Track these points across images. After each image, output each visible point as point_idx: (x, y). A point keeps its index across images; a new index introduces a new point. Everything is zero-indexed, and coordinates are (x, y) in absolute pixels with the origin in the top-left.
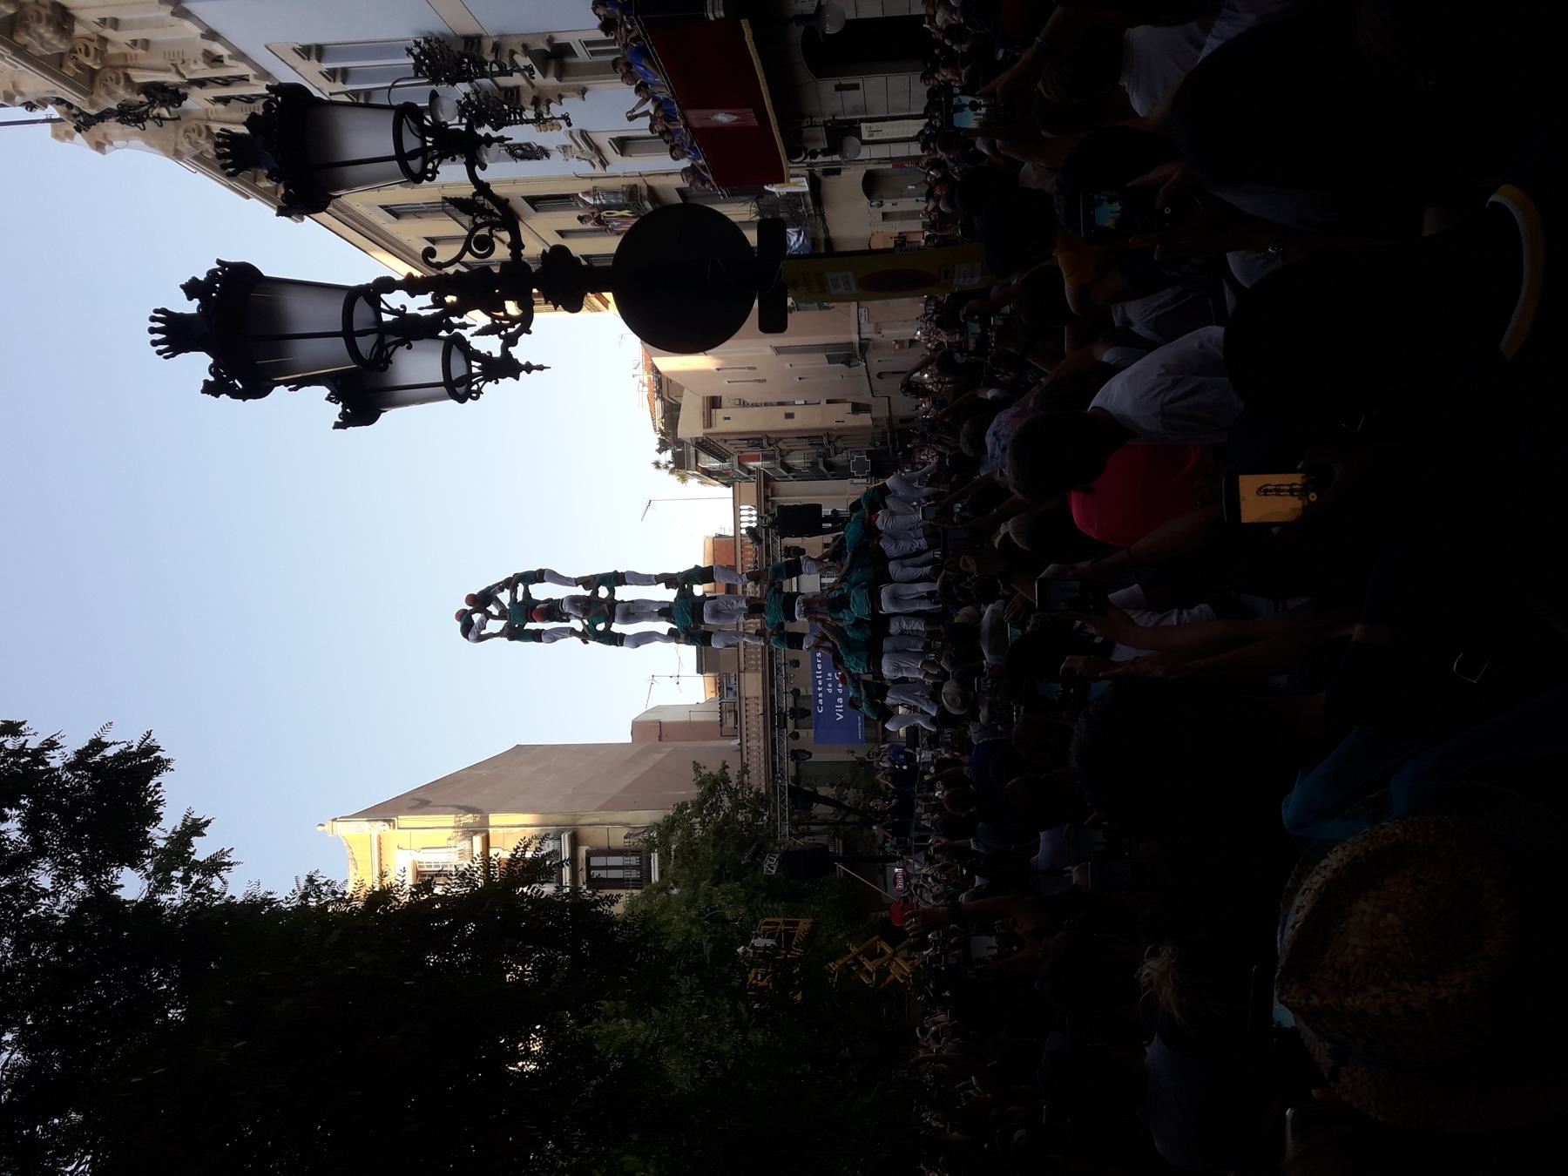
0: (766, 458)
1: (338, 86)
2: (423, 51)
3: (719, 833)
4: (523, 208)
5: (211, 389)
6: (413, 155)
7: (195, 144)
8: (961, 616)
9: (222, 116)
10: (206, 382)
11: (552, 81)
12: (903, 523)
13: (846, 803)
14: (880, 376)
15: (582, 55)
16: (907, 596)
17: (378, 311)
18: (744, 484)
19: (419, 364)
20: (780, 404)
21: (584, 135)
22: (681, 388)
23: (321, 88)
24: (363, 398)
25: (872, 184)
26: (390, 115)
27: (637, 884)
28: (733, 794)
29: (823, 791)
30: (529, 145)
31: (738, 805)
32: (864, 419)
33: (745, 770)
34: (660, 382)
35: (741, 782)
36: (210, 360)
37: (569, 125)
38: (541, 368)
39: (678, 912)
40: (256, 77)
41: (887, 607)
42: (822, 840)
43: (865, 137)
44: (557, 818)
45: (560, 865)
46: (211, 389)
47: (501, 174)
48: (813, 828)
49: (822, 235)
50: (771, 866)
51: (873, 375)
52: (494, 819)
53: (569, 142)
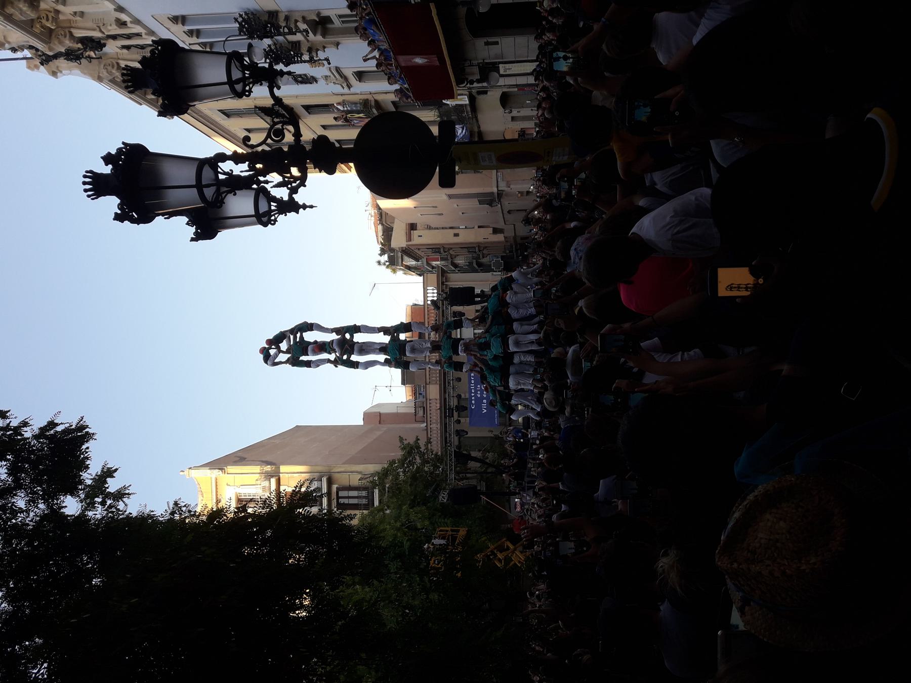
0: (442, 259)
1: (194, 40)
2: (244, 20)
3: (414, 478)
4: (302, 112)
5: (119, 218)
6: (238, 81)
7: (110, 73)
8: (555, 353)
9: (125, 57)
10: (116, 213)
11: (319, 38)
12: (521, 298)
13: (487, 461)
14: (509, 212)
15: (337, 23)
16: (524, 341)
17: (217, 173)
18: (429, 275)
19: (240, 204)
20: (451, 228)
21: (338, 69)
22: (393, 218)
23: (184, 42)
24: (207, 224)
25: (505, 100)
26: (224, 59)
27: (366, 507)
28: (422, 455)
29: (474, 454)
30: (305, 75)
31: (425, 462)
32: (500, 238)
33: (429, 441)
34: (381, 215)
35: (427, 448)
36: (119, 201)
37: (329, 63)
38: (311, 207)
39: (390, 524)
40: (146, 34)
41: (512, 348)
42: (474, 482)
43: (502, 72)
44: (320, 469)
45: (321, 496)
46: (119, 218)
47: (289, 92)
48: (468, 475)
49: (476, 129)
50: (443, 497)
51: (505, 212)
52: (283, 469)
53: (329, 73)
